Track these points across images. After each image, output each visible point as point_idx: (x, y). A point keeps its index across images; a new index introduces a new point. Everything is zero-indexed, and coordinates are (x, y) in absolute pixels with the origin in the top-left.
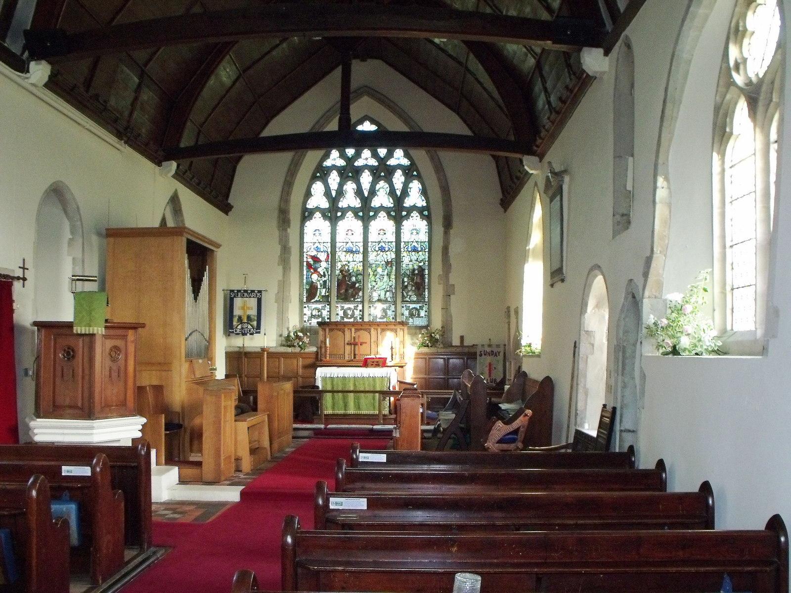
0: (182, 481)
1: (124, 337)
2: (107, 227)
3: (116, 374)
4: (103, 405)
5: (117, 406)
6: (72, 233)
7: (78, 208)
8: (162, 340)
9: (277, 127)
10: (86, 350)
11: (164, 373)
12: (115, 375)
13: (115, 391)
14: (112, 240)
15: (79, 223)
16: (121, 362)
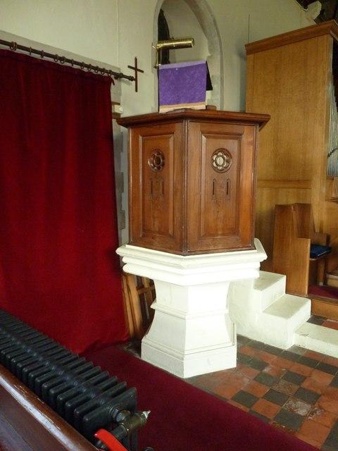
0: (316, 319)
1: (238, 136)
2: (246, 43)
3: (224, 190)
4: (202, 234)
5: (223, 234)
6: (210, 50)
7: (214, 21)
8: (301, 156)
9: (336, 152)
10: (177, 155)
11: (302, 191)
12: (221, 191)
13: (221, 214)
14: (251, 56)
15: (217, 38)
16: (232, 175)
